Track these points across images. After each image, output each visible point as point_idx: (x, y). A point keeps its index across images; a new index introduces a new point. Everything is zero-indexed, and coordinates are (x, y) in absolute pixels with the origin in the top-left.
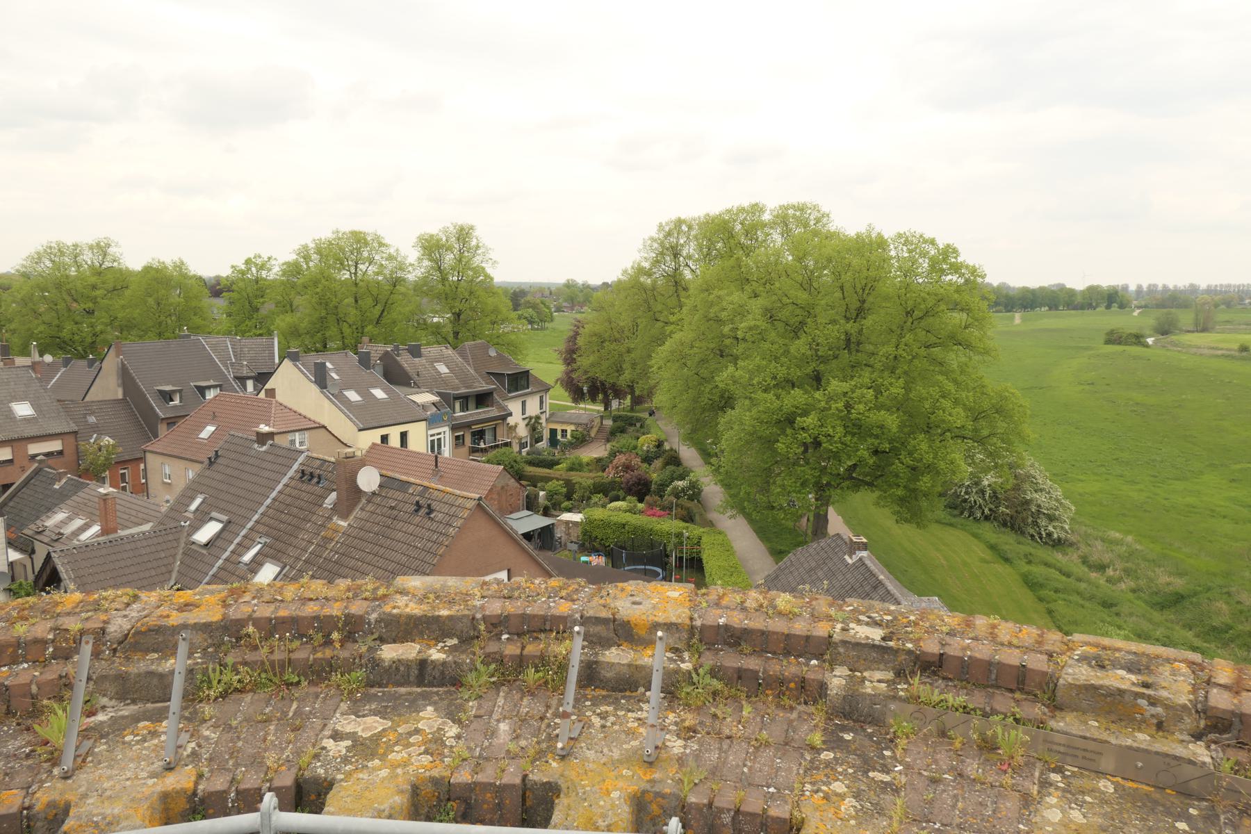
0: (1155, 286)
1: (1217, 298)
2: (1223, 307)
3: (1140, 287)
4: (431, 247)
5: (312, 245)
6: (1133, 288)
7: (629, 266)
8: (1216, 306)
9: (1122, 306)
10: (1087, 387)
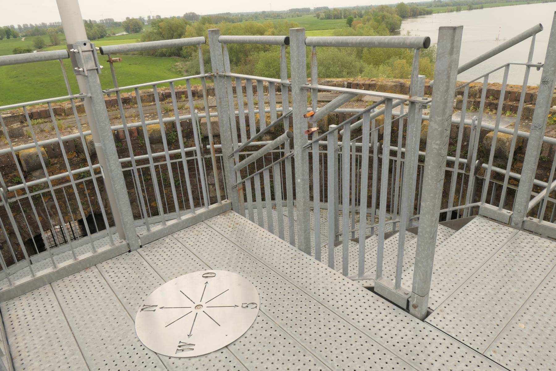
0: (26, 25)
1: (56, 29)
2: (60, 33)
3: (19, 26)
4: (24, 25)
5: (146, 19)
6: (16, 27)
7: (155, 15)
8: (57, 32)
9: (15, 36)
10: (15, 79)
